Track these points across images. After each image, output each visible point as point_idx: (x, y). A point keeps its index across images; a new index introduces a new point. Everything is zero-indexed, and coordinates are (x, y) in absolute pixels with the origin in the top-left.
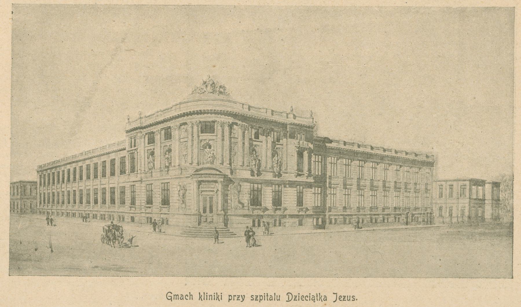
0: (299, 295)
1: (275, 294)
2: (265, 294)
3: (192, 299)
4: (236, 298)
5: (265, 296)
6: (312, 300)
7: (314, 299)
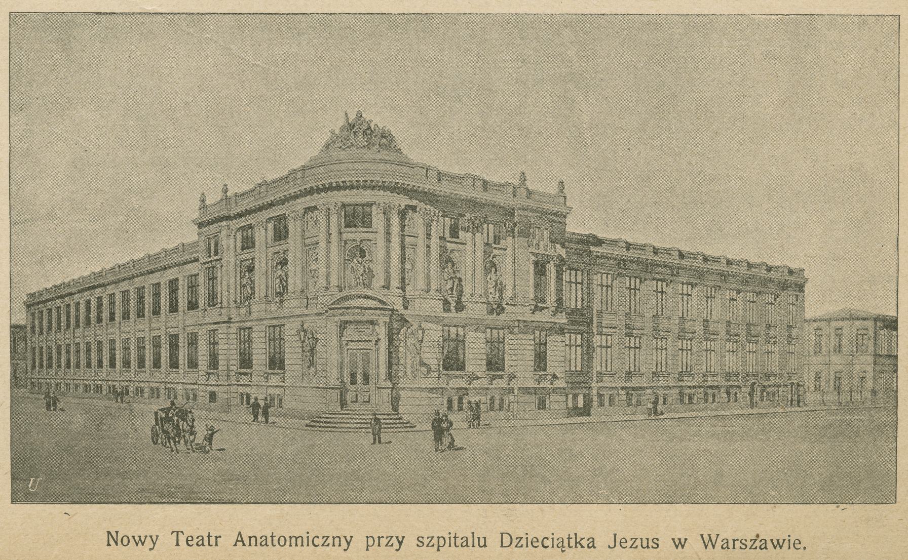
1: (473, 533)
3: (702, 536)
5: (450, 538)
7: (563, 546)
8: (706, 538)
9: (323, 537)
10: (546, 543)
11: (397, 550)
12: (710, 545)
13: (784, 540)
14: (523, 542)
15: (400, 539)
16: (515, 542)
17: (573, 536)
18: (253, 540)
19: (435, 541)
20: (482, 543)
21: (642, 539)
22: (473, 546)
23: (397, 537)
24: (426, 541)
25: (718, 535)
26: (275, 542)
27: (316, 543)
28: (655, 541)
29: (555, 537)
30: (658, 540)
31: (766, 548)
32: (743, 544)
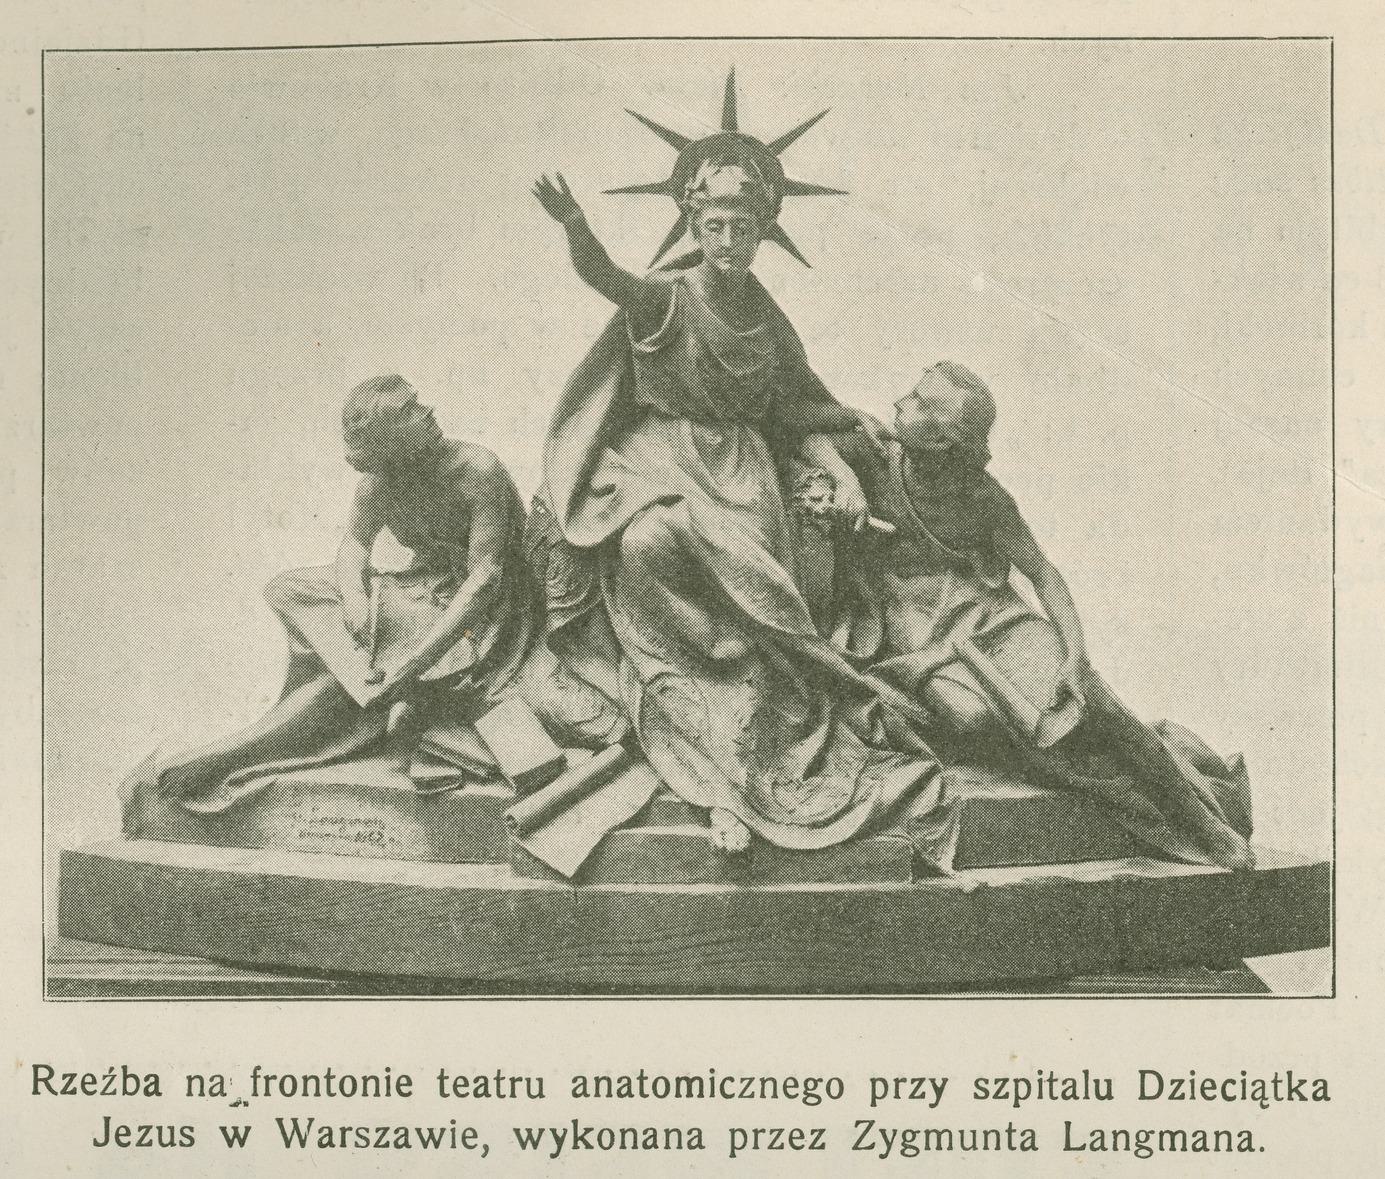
0: (452, 1126)
1: (1086, 1072)
2: (1040, 1072)
3: (280, 1121)
4: (906, 1089)
5: (1040, 1081)
6: (1254, 1098)
7: (1263, 1097)
8: (289, 1127)
9: (743, 1080)
10: (1231, 1090)
11: (932, 1106)
12: (295, 1140)
13: (443, 1130)
14: (1186, 1088)
15: (939, 1084)
16: (1168, 1089)
17: (1283, 1076)
18: (604, 1084)
19: (1010, 1087)
20: (1103, 1092)
21: (160, 1129)
22: (1087, 1097)
23: (933, 1081)
24: (992, 1088)
25: (311, 1120)
26: (648, 1089)
27: (728, 1091)
28: (187, 1131)
29: (1249, 1080)
30: (191, 1129)
31: (407, 1145)
32: (361, 1137)
